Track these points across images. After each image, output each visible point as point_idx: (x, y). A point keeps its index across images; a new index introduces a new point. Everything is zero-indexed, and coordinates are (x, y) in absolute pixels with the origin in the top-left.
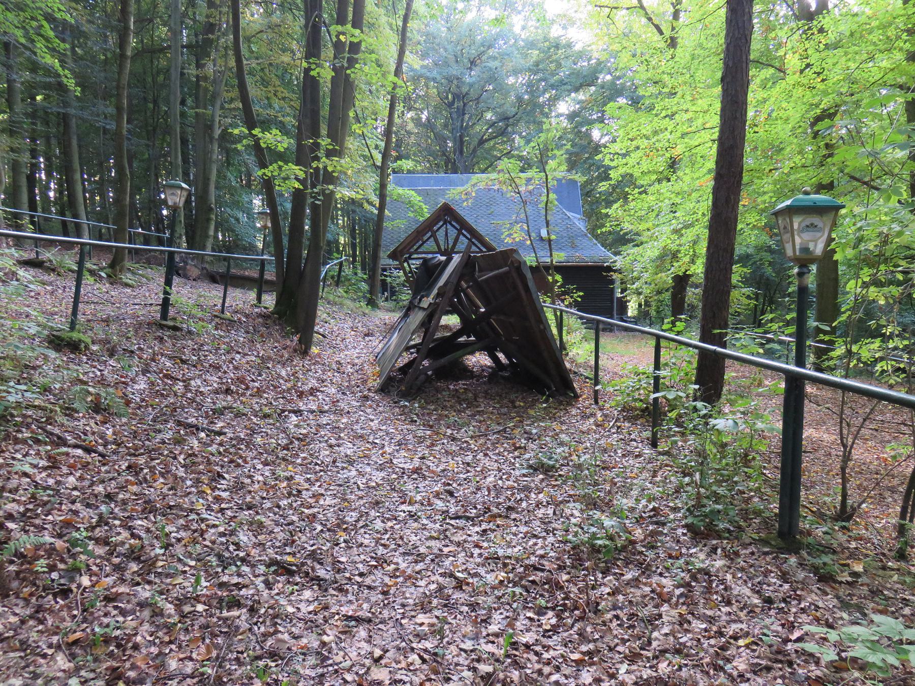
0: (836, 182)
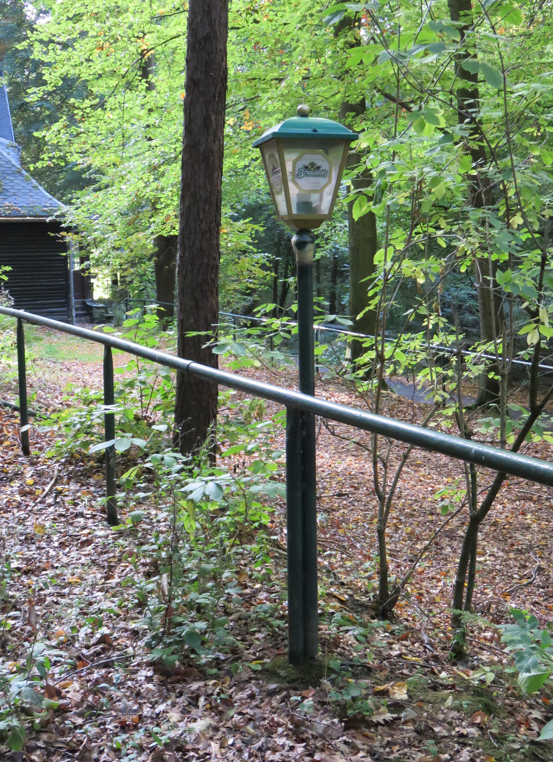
0: (368, 103)
